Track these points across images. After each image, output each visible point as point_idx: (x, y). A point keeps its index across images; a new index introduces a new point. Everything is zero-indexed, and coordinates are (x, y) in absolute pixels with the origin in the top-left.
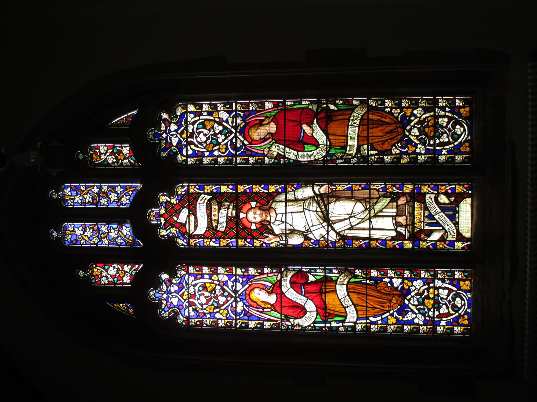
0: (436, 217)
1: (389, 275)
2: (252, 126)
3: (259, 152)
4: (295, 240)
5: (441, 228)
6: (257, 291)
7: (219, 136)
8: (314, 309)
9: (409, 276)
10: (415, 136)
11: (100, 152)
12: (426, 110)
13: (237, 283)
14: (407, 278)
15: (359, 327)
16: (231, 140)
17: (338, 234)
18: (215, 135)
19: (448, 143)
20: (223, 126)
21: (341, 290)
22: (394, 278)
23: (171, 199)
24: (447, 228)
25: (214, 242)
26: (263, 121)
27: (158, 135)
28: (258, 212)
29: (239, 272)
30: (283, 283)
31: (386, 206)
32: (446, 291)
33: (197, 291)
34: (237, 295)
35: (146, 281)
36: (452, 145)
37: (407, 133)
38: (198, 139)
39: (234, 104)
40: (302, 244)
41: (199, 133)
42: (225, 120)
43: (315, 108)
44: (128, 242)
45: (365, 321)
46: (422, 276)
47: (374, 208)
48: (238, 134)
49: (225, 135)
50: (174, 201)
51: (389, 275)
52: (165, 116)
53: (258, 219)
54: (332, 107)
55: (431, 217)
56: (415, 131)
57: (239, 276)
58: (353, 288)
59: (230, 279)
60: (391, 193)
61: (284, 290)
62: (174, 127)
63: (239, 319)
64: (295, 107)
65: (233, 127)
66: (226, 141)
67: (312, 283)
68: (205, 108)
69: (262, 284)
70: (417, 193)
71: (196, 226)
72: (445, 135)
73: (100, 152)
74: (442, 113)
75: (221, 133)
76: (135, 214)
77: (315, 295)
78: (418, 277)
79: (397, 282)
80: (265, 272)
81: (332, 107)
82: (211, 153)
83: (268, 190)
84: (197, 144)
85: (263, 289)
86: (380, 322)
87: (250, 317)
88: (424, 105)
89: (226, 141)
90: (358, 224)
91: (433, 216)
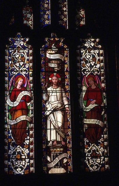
0: (57, 158)
1: (31, 139)
2: (94, 78)
3: (83, 81)
4: (45, 97)
5: (52, 160)
6: (22, 80)
7: (89, 64)
8: (15, 106)
9: (31, 148)
10: (92, 148)
11: (81, 11)
12: (103, 153)
13: (25, 72)
14: (29, 147)
15: (6, 126)
16: (87, 69)
17: (48, 116)
18: (90, 62)
19: (89, 163)
20: (93, 66)
21: (23, 118)
22: (29, 141)
23: (62, 43)
24: (52, 163)
25: (43, 61)
26: (96, 83)
27: (19, 37)
28: (56, 81)
29: (31, 73)
30: (26, 92)
31: (61, 136)
32: (24, 164)
33: (21, 53)
34: (20, 72)
35: (26, 32)
36: (88, 164)
37: (92, 145)
38: (88, 55)
39: (103, 70)
40: (43, 100)
41: (90, 55)
42: (96, 66)
43: (102, 105)
44: (42, 23)
45: (9, 128)
46: (31, 153)
47: (60, 131)
48: (90, 72)
49: (19, 67)
50: (61, 44)
51: (31, 139)
52: (97, 40)
53: (54, 81)
54: (103, 112)
55: (57, 156)
56: (94, 148)
57: (29, 73)
58: (24, 123)
59: (27, 68)
60: (67, 138)
61: (23, 92)
62: (93, 44)
63: (9, 73)
64: (103, 97)
65: (93, 70)
66: (87, 67)
67: (26, 105)
68: (101, 58)
69: (25, 83)
70: (67, 149)
71: (50, 54)
72: (92, 161)
73: (81, 11)
74: (102, 160)
75: (91, 65)
76: (56, 27)
77: (21, 106)
78: (31, 151)
79: (27, 142)
80: (31, 84)
81: (103, 112)
82: (10, 60)
83: (66, 85)
84: (86, 54)
85: (23, 83)
86: (9, 135)
87: (10, 78)
88: (105, 151)
89: (87, 67)
90: (53, 124)
91: (57, 157)
